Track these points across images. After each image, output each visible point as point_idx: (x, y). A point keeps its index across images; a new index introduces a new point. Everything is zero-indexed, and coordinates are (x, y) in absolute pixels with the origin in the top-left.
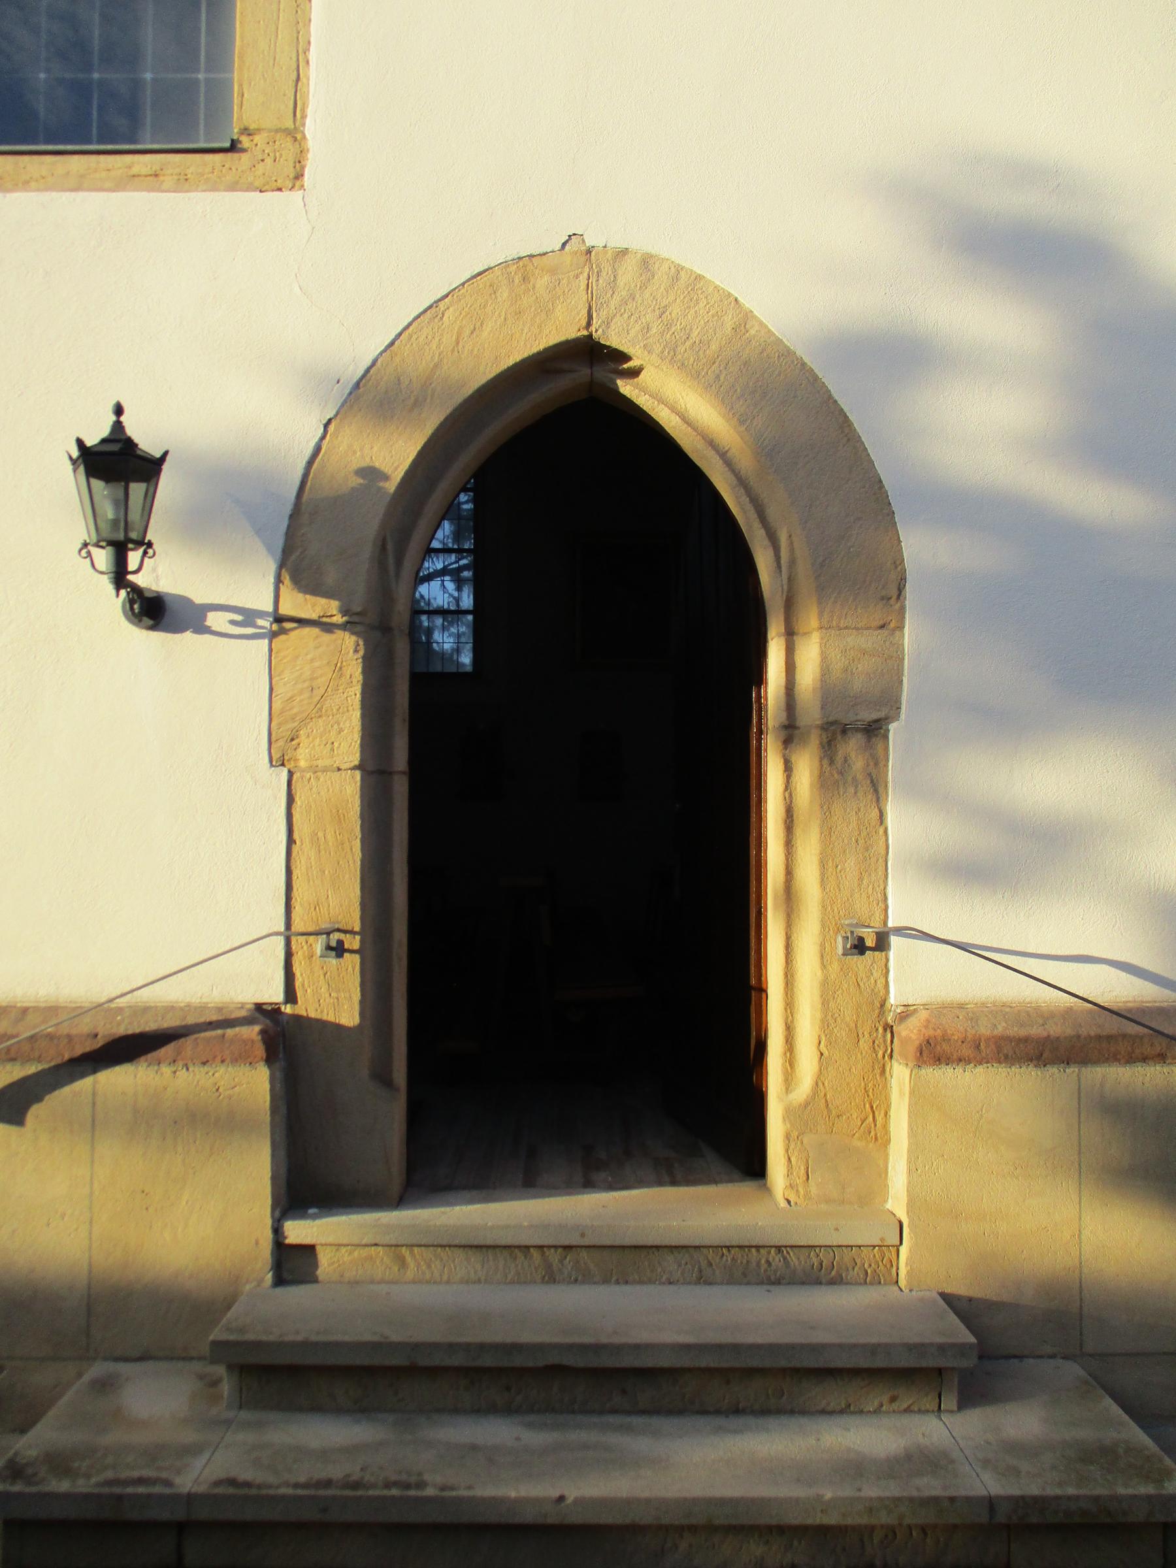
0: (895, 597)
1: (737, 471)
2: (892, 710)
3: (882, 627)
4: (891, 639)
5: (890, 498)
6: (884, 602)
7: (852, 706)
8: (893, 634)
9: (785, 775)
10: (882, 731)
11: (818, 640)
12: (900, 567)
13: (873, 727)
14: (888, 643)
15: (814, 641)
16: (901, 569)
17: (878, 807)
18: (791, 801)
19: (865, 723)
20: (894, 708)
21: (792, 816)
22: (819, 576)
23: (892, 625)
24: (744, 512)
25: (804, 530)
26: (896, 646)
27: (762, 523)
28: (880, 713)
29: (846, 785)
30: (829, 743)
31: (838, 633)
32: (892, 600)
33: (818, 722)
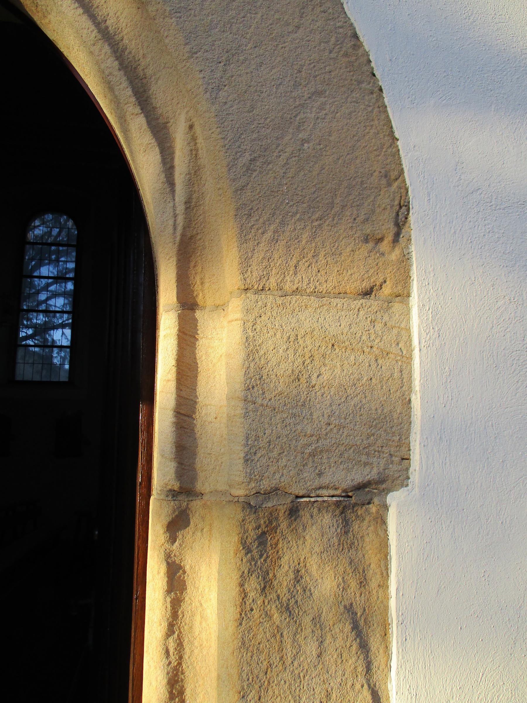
0: (390, 238)
1: (99, 18)
2: (392, 462)
3: (367, 293)
4: (386, 318)
5: (373, 64)
6: (370, 245)
7: (312, 455)
8: (388, 308)
9: (169, 600)
10: (373, 509)
11: (238, 315)
12: (396, 184)
13: (353, 500)
14: (379, 326)
15: (232, 316)
16: (400, 188)
17: (369, 685)
18: (181, 657)
19: (338, 492)
20: (396, 459)
21: (181, 692)
22: (243, 188)
23: (387, 290)
24: (110, 87)
25: (213, 104)
26: (395, 331)
27: (140, 104)
28: (368, 469)
29: (300, 638)
30: (262, 539)
31: (279, 301)
32: (386, 242)
33: (240, 492)
